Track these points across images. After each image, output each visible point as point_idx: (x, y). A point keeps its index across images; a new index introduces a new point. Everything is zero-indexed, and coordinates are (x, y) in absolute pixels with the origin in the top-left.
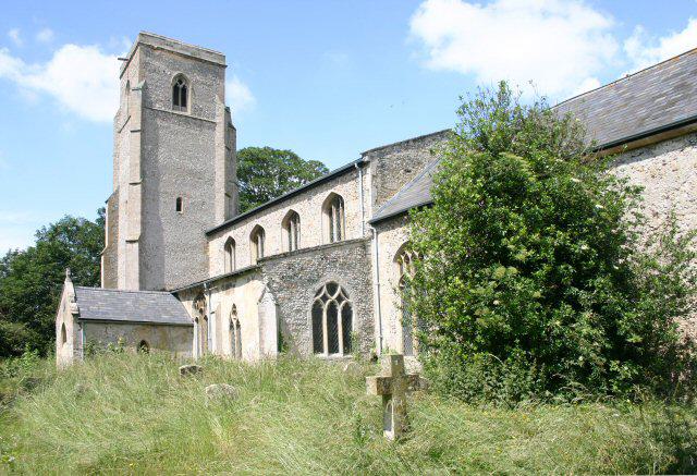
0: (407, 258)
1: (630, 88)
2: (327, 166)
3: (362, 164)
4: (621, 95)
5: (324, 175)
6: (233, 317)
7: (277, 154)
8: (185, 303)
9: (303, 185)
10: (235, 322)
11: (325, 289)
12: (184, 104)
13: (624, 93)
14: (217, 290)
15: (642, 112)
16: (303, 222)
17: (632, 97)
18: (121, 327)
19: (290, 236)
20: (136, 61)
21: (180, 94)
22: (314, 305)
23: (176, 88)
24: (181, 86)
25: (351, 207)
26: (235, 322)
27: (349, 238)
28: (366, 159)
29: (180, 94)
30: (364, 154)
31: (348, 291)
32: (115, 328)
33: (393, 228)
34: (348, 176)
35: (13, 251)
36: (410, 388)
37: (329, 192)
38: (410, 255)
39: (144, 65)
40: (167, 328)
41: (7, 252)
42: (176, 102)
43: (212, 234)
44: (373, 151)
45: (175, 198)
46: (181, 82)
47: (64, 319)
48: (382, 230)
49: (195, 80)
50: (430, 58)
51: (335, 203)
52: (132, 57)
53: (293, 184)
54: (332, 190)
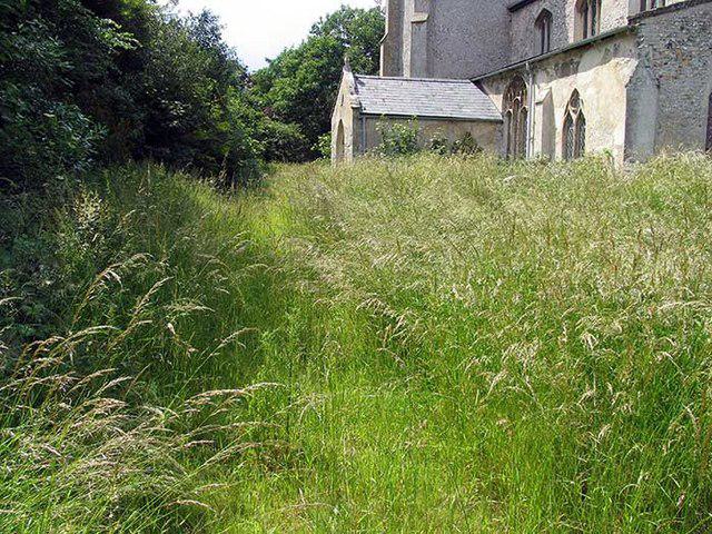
10: (574, 117)
26: (574, 117)
40: (468, 126)
47: (342, 116)
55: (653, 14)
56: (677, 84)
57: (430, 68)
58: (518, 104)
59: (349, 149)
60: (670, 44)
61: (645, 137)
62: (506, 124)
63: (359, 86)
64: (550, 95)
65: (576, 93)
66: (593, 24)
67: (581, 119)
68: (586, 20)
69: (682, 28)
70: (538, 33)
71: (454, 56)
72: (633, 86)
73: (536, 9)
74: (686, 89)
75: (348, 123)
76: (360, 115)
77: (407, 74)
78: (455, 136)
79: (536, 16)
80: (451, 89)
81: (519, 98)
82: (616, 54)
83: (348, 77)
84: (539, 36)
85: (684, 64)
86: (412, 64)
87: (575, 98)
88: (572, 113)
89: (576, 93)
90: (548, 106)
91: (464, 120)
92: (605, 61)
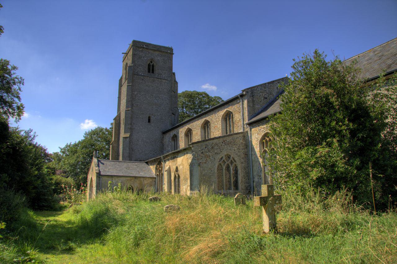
0: (267, 142)
1: (381, 51)
2: (223, 99)
3: (242, 96)
4: (376, 55)
5: (221, 103)
6: (176, 173)
7: (199, 94)
8: (151, 167)
9: (211, 108)
10: (177, 176)
11: (224, 158)
12: (153, 72)
13: (378, 53)
14: (168, 160)
15: (389, 62)
16: (212, 125)
17: (383, 55)
18: (119, 178)
19: (175, 143)
20: (131, 53)
21: (151, 69)
22: (218, 166)
23: (149, 65)
24: (151, 64)
25: (237, 117)
26: (177, 176)
27: (212, 137)
28: (244, 93)
29: (151, 69)
30: (243, 91)
31: (236, 159)
32: (117, 179)
33: (259, 126)
34: (235, 102)
35: (69, 144)
36: (277, 202)
37: (226, 110)
38: (268, 139)
39: (134, 55)
40: (142, 179)
41: (66, 144)
42: (149, 72)
43: (164, 133)
44: (248, 89)
45: (147, 116)
46: (151, 62)
47: (92, 176)
48: (253, 127)
49: (158, 58)
50: (11, 132)
51: (228, 117)
52: (129, 52)
53: (206, 108)
54: (205, 119)
55: (229, 135)
56: (205, 165)
57: (130, 157)
58: (160, 171)
59: (94, 189)
60: (202, 152)
61: (196, 182)
62: (157, 179)
63: (100, 164)
64: (170, 168)
65: (177, 168)
66: (177, 144)
67: (179, 176)
68: (188, 139)
69: (206, 148)
70: (173, 143)
71: (140, 151)
72: (192, 165)
73: (172, 133)
74: (209, 166)
75: (95, 179)
76: (99, 175)
77: (121, 158)
78: (136, 185)
79: (172, 136)
80: (136, 165)
81: (160, 169)
82: (187, 154)
83: (95, 160)
84: (173, 144)
85: (208, 159)
86: (123, 154)
87: (177, 170)
88: (176, 175)
89: (177, 168)
90: (169, 172)
91: (140, 177)
92: (185, 154)
